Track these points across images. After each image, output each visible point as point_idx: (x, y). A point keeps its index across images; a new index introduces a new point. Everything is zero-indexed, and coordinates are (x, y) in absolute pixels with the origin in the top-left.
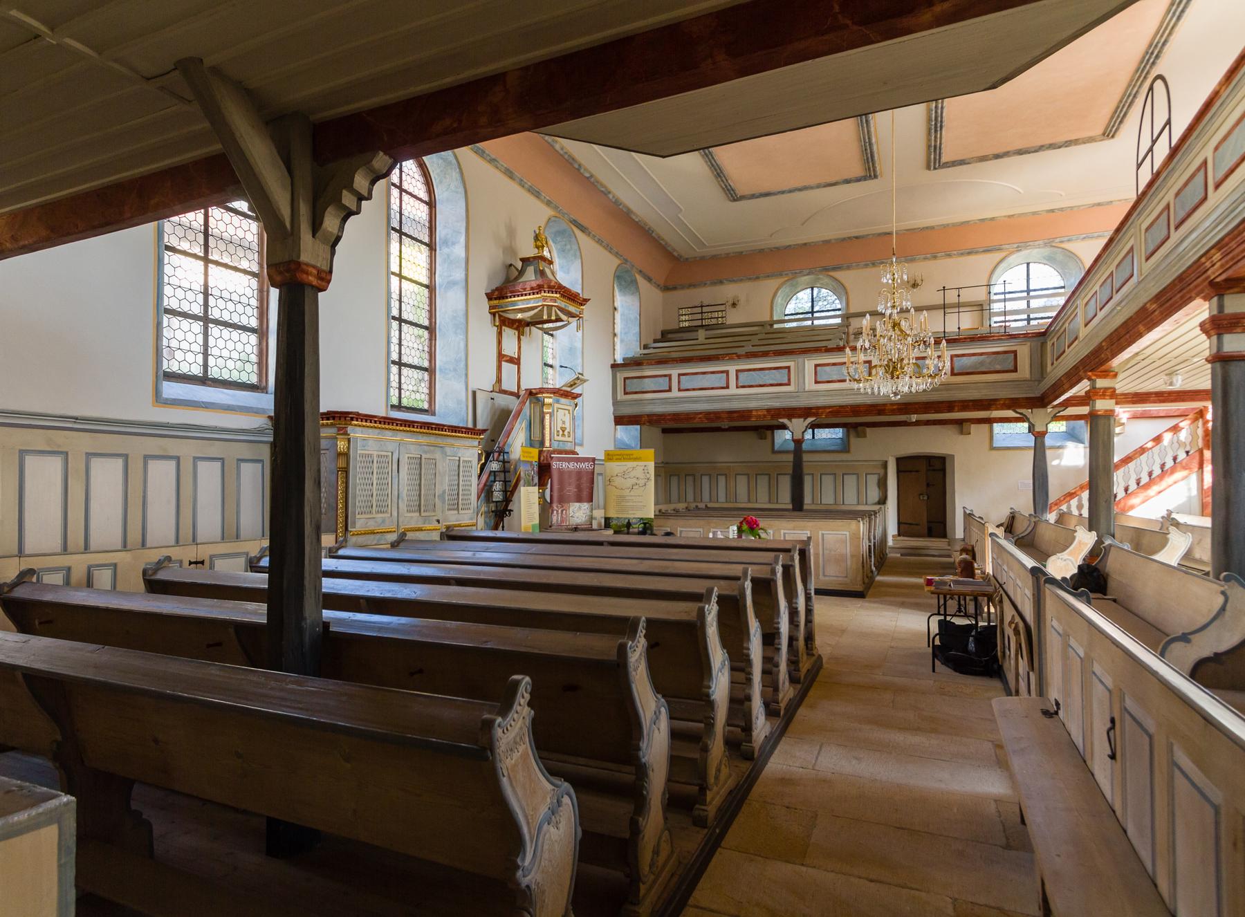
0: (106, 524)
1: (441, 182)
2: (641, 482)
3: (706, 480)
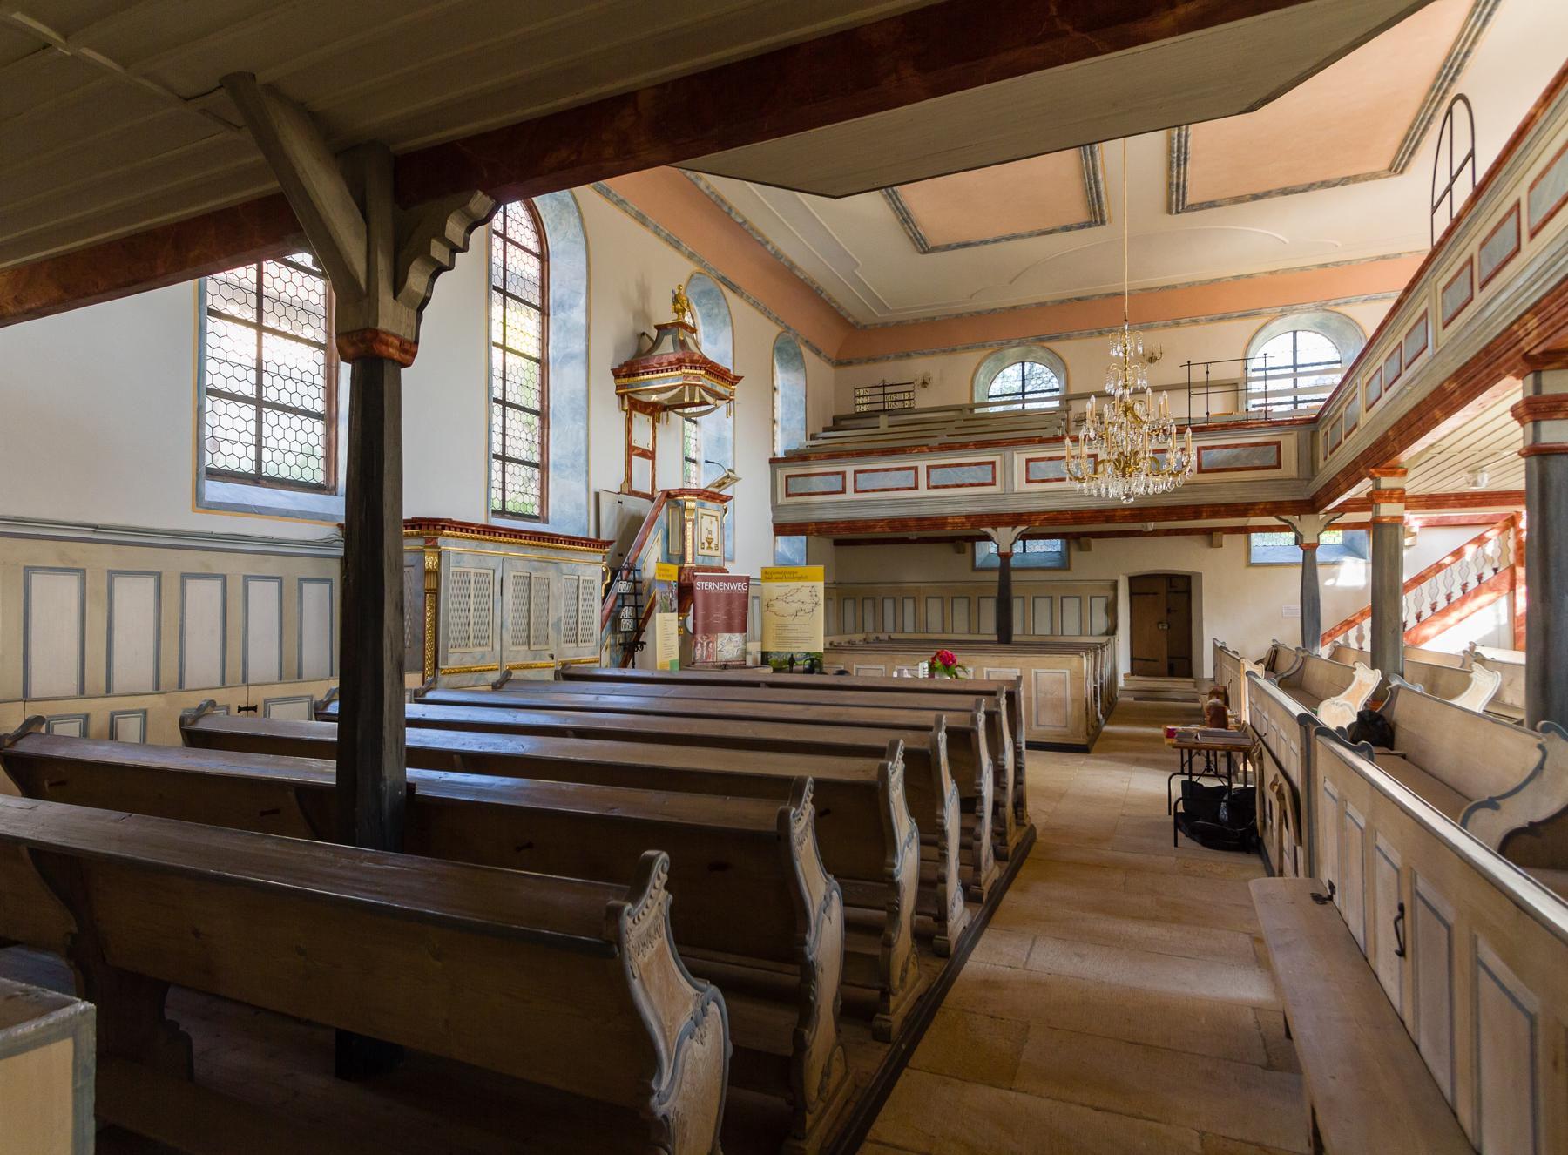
0: (134, 660)
1: (555, 229)
2: (808, 607)
3: (889, 604)
